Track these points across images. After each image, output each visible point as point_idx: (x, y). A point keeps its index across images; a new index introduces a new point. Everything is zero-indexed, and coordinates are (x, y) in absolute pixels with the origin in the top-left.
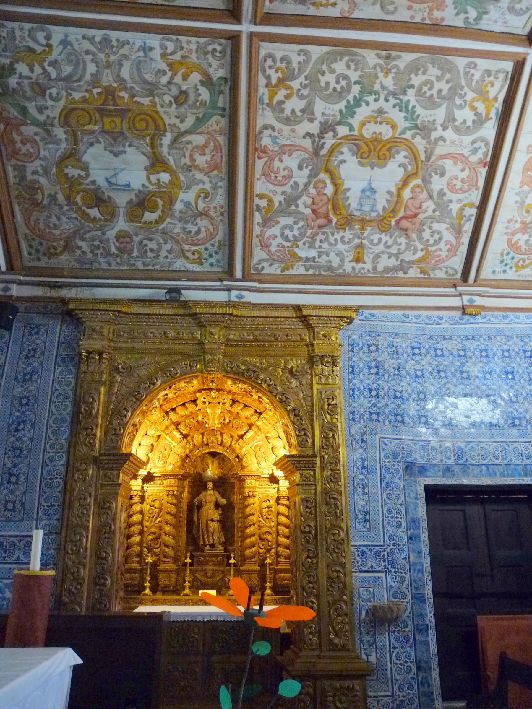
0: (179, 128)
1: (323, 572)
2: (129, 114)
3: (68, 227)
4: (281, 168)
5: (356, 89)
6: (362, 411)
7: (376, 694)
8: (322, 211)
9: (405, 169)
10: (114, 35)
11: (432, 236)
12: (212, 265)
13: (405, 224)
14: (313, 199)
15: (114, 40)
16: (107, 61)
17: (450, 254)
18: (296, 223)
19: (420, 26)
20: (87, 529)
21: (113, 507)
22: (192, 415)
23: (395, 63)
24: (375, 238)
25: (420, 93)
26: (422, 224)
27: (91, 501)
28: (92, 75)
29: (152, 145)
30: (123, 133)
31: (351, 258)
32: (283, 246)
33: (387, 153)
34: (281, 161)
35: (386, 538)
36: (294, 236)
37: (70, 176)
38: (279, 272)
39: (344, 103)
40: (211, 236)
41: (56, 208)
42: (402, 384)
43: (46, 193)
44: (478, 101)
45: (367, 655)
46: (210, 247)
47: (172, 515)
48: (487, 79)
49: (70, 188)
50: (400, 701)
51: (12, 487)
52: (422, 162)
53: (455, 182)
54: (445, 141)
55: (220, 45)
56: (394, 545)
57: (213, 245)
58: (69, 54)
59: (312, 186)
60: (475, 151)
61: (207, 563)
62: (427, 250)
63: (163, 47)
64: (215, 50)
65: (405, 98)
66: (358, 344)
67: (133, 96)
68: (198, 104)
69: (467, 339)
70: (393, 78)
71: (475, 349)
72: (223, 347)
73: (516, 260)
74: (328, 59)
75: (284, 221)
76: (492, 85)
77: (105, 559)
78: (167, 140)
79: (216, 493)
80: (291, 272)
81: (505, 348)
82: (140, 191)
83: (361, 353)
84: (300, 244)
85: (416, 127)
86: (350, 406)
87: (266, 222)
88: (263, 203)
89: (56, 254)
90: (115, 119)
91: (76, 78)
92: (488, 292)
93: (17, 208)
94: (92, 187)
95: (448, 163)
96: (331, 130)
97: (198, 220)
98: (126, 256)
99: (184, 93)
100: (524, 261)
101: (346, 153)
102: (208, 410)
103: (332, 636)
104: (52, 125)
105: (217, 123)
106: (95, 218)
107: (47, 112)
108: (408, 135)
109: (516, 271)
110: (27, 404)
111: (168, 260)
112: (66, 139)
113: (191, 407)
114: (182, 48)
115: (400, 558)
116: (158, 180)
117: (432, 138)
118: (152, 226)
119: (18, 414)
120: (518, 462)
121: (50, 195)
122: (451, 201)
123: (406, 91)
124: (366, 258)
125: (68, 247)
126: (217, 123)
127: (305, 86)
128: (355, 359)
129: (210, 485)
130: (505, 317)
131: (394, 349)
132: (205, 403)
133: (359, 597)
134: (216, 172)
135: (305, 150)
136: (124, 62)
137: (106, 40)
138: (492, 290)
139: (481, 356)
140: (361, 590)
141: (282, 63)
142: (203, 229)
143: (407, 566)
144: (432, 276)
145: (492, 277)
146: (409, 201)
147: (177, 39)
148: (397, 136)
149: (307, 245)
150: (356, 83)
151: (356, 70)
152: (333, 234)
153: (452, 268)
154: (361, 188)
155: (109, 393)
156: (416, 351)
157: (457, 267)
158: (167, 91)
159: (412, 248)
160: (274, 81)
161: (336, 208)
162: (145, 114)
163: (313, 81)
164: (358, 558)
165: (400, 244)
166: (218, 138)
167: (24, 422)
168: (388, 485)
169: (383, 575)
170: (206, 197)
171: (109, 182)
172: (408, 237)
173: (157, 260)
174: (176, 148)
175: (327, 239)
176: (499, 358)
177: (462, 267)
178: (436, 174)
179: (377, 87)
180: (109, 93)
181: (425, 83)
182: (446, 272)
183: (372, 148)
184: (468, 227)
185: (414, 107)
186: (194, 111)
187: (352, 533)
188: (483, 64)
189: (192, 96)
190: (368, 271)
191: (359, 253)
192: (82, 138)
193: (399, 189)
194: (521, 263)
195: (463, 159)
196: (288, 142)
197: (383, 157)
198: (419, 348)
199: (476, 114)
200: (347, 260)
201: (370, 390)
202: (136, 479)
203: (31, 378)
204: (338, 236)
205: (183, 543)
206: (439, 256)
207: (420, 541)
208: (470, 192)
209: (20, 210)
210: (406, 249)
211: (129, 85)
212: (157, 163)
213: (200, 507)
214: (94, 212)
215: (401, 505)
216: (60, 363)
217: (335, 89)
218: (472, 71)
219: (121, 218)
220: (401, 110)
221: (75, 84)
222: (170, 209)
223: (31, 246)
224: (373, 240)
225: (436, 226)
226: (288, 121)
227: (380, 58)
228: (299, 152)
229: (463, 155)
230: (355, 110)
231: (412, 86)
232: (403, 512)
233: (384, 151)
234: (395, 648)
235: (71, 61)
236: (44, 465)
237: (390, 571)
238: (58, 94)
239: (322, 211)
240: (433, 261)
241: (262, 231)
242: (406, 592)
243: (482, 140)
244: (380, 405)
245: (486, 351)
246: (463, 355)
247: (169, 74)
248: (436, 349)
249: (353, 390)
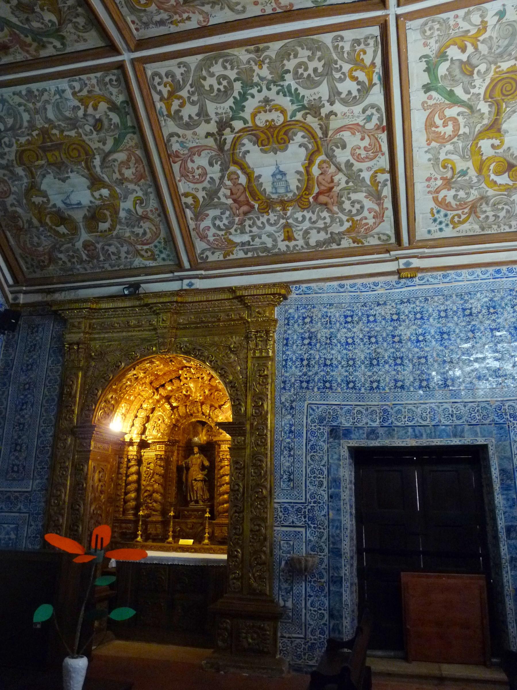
0: (103, 150)
1: (247, 526)
2: (64, 147)
3: (47, 244)
4: (195, 168)
5: (238, 86)
6: (293, 380)
7: (290, 635)
8: (242, 198)
9: (307, 149)
10: (34, 86)
11: (353, 206)
12: (164, 259)
13: (323, 199)
14: (231, 189)
15: (35, 90)
16: (35, 108)
17: (378, 221)
18: (222, 213)
19: (273, 16)
20: (65, 485)
21: (86, 470)
22: (179, 389)
23: (265, 54)
24: (299, 215)
25: (297, 76)
26: (339, 196)
27: (69, 464)
28: (28, 122)
29: (88, 168)
30: (63, 163)
31: (282, 238)
32: (218, 235)
33: (285, 137)
34: (193, 161)
35: (308, 496)
36: (224, 225)
37: (37, 203)
38: (221, 258)
39: (231, 100)
40: (157, 235)
41: (34, 230)
42: (333, 352)
43: (25, 219)
44: (356, 70)
45: (284, 601)
46: (157, 244)
47: (160, 475)
48: (358, 48)
49: (39, 212)
50: (312, 643)
51: (17, 454)
52: (321, 138)
53: (358, 151)
54: (336, 115)
55: (114, 75)
56: (315, 502)
57: (159, 242)
58: (8, 109)
59: (226, 178)
60: (369, 119)
61: (189, 517)
62: (353, 221)
63: (72, 87)
64: (111, 80)
65: (286, 84)
66: (293, 317)
67: (62, 131)
68: (112, 127)
69: (402, 302)
70: (268, 67)
71: (410, 312)
72: (174, 331)
73: (449, 217)
74: (205, 65)
75: (212, 213)
76: (365, 53)
77: (78, 510)
78: (97, 162)
79: (202, 456)
80: (232, 257)
81: (442, 308)
82: (89, 207)
83: (296, 326)
84: (232, 231)
85: (304, 107)
86: (282, 376)
87: (199, 216)
88: (189, 200)
89: (45, 266)
90: (54, 153)
91: (17, 127)
92: (424, 253)
93: (8, 234)
94: (54, 209)
95: (346, 135)
96: (227, 127)
97: (142, 224)
98: (95, 261)
99: (99, 121)
100: (459, 217)
101: (248, 144)
102: (192, 385)
103: (252, 581)
104: (13, 166)
105: (131, 140)
106: (64, 233)
107: (7, 157)
108: (299, 116)
109: (453, 228)
110: (29, 389)
111: (129, 260)
112: (26, 175)
113: (176, 383)
114: (86, 85)
115: (320, 515)
116: (101, 195)
117: (323, 115)
118: (107, 233)
119: (22, 397)
120: (448, 423)
121: (27, 221)
122: (361, 170)
123: (284, 77)
124: (296, 236)
125: (52, 260)
126: (132, 139)
127: (193, 93)
128: (289, 332)
129: (196, 450)
130: (445, 276)
131: (328, 319)
132: (186, 378)
133: (280, 549)
134: (143, 180)
135: (210, 148)
136: (47, 106)
137: (30, 92)
138: (426, 250)
139: (416, 319)
140: (282, 542)
141: (167, 78)
142: (148, 231)
144: (366, 244)
145: (429, 237)
146: (320, 178)
147: (80, 79)
148: (289, 119)
149: (239, 231)
150: (235, 80)
151: (232, 69)
152: (259, 219)
153: (384, 234)
154: (271, 173)
155: (85, 376)
156: (349, 319)
157: (388, 232)
158: (86, 122)
159: (338, 220)
160: (166, 95)
161: (254, 195)
162: (74, 144)
163: (198, 87)
164: (281, 514)
165: (325, 218)
166: (137, 152)
167: (26, 403)
168: (313, 447)
169: (303, 530)
170: (141, 203)
171: (65, 203)
172: (329, 210)
173: (120, 261)
174: (107, 167)
175: (254, 223)
176: (434, 319)
177: (393, 231)
178: (338, 147)
179: (256, 79)
180: (45, 133)
181: (299, 65)
182: (379, 238)
183: (270, 135)
184: (387, 191)
185: (296, 89)
186: (111, 134)
187: (277, 491)
188: (349, 35)
189: (106, 122)
190: (302, 247)
191: (288, 232)
192: (36, 173)
193: (306, 167)
194: (456, 219)
195: (360, 128)
196: (195, 144)
197: (283, 141)
198: (352, 316)
199: (359, 83)
200: (279, 240)
201: (302, 360)
202: (133, 446)
203: (31, 368)
204: (264, 219)
205: (172, 499)
206: (367, 224)
207: (340, 500)
208: (377, 158)
209: (12, 235)
210: (332, 221)
211: (57, 124)
212: (95, 183)
213: (188, 469)
214: (62, 229)
215: (324, 466)
216: (52, 354)
217: (219, 90)
218: (341, 44)
219: (83, 231)
220: (285, 95)
221: (19, 132)
222: (117, 217)
223: (26, 263)
224: (297, 218)
225: (354, 196)
226: (188, 126)
227: (250, 53)
228: (206, 151)
229: (358, 124)
230: (244, 104)
231: (288, 71)
232: (326, 472)
233: (281, 135)
234: (310, 596)
235: (10, 114)
236: (39, 436)
237: (310, 527)
238: (9, 141)
239: (242, 198)
240: (363, 230)
241: (196, 225)
242: (324, 547)
243: (372, 106)
244: (310, 373)
245: (421, 313)
246: (397, 319)
247: (82, 108)
248: (368, 316)
249: (286, 360)
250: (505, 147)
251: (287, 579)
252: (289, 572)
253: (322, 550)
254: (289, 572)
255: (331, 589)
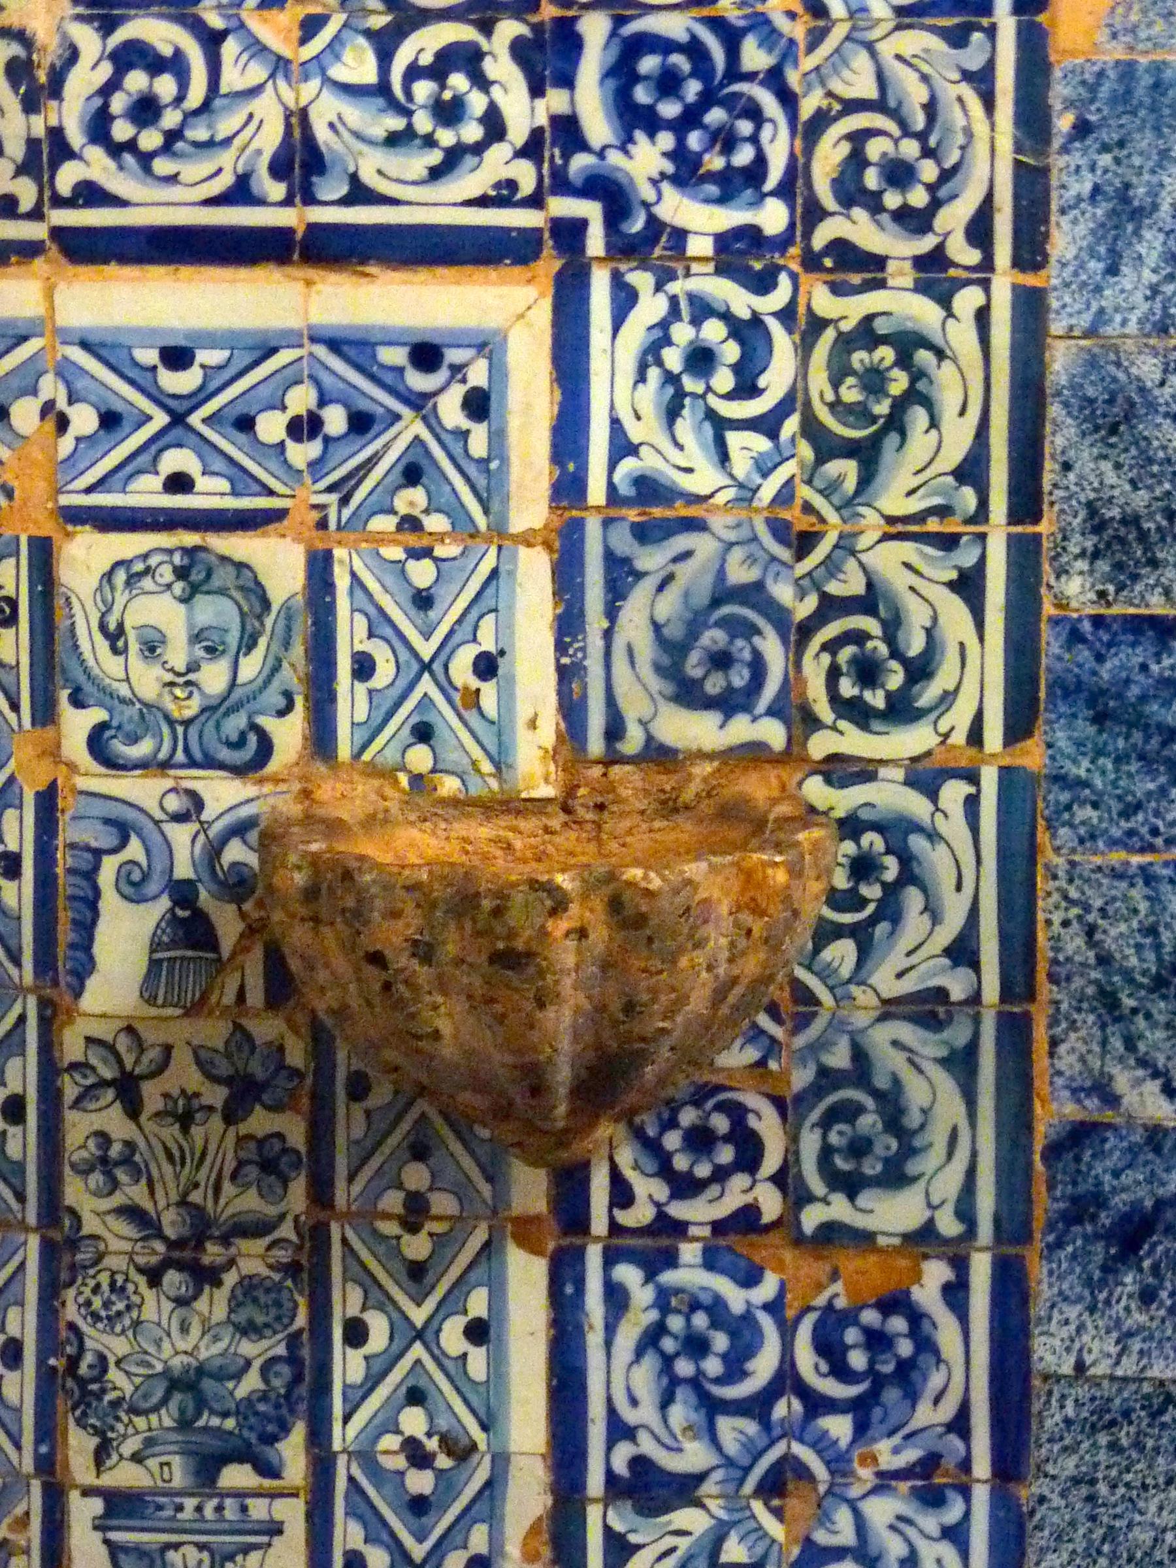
140: (86, 557)
143: (990, 150)
169: (509, 308)
237: (650, 245)
242: (925, 599)
251: (201, 1225)
252: (244, 1094)
253: (887, 678)
254: (244, 1094)
255: (1049, 1352)
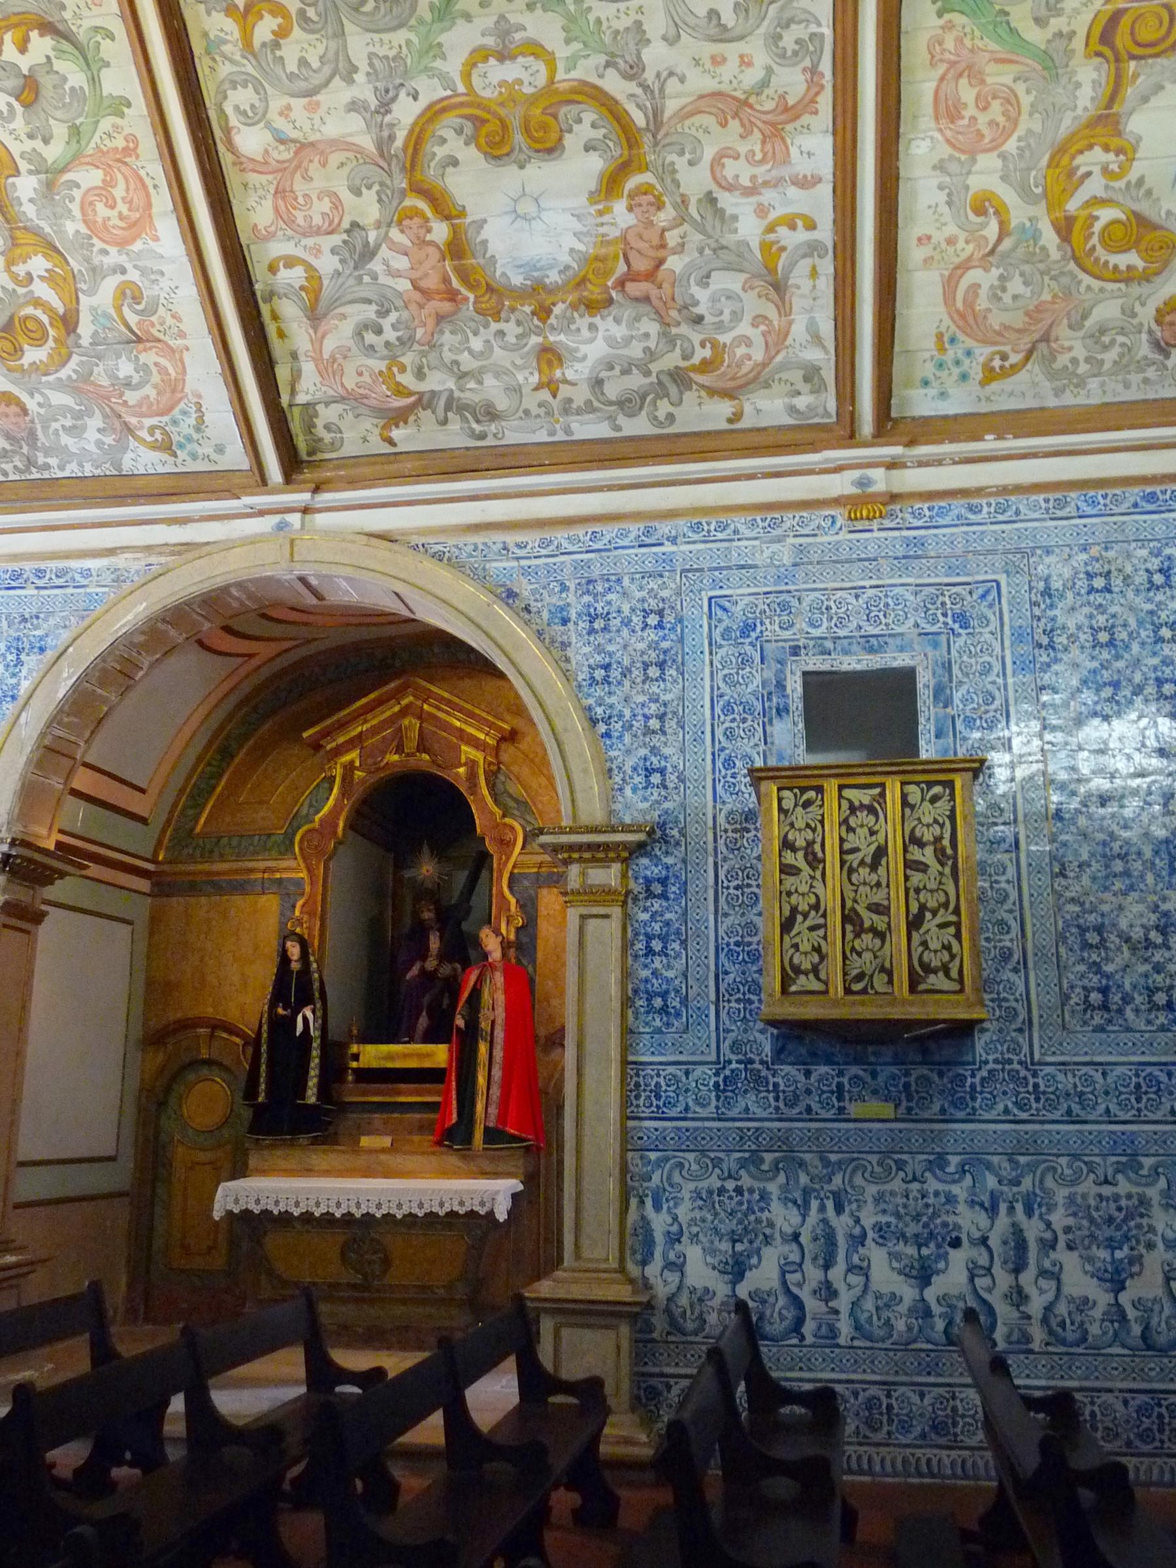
88: (292, 277)
100: (1004, 357)
101: (451, 142)
250: (1133, 176)
